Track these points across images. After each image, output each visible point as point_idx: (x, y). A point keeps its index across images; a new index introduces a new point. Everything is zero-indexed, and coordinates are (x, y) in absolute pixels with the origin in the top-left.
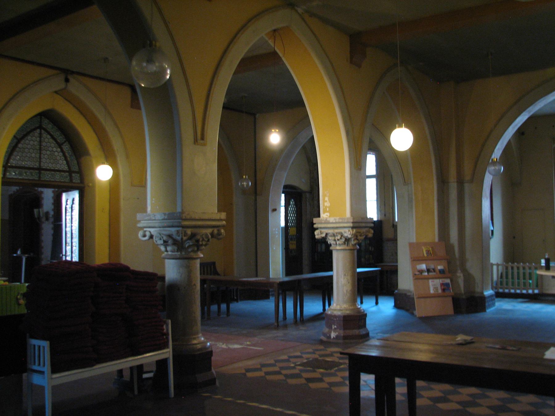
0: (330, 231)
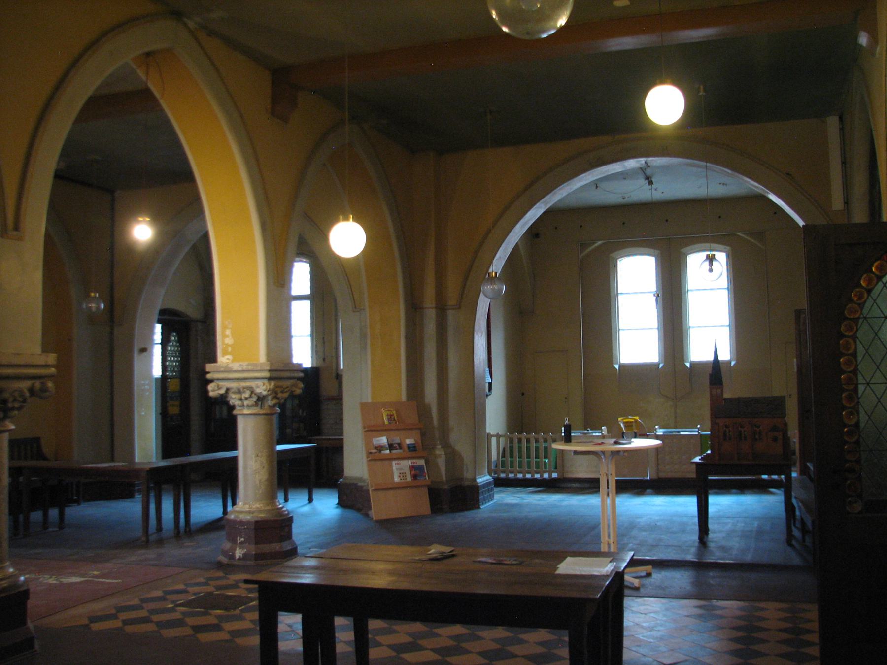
0: (234, 385)
